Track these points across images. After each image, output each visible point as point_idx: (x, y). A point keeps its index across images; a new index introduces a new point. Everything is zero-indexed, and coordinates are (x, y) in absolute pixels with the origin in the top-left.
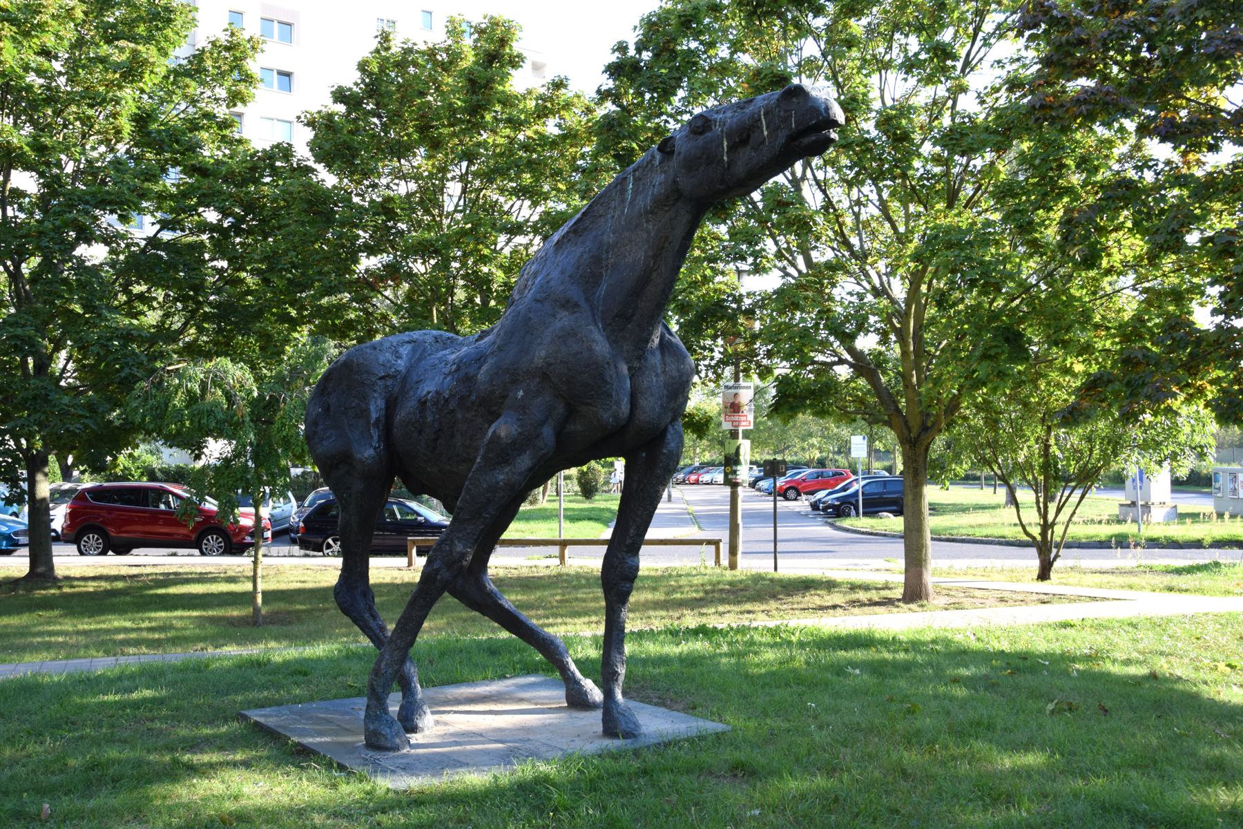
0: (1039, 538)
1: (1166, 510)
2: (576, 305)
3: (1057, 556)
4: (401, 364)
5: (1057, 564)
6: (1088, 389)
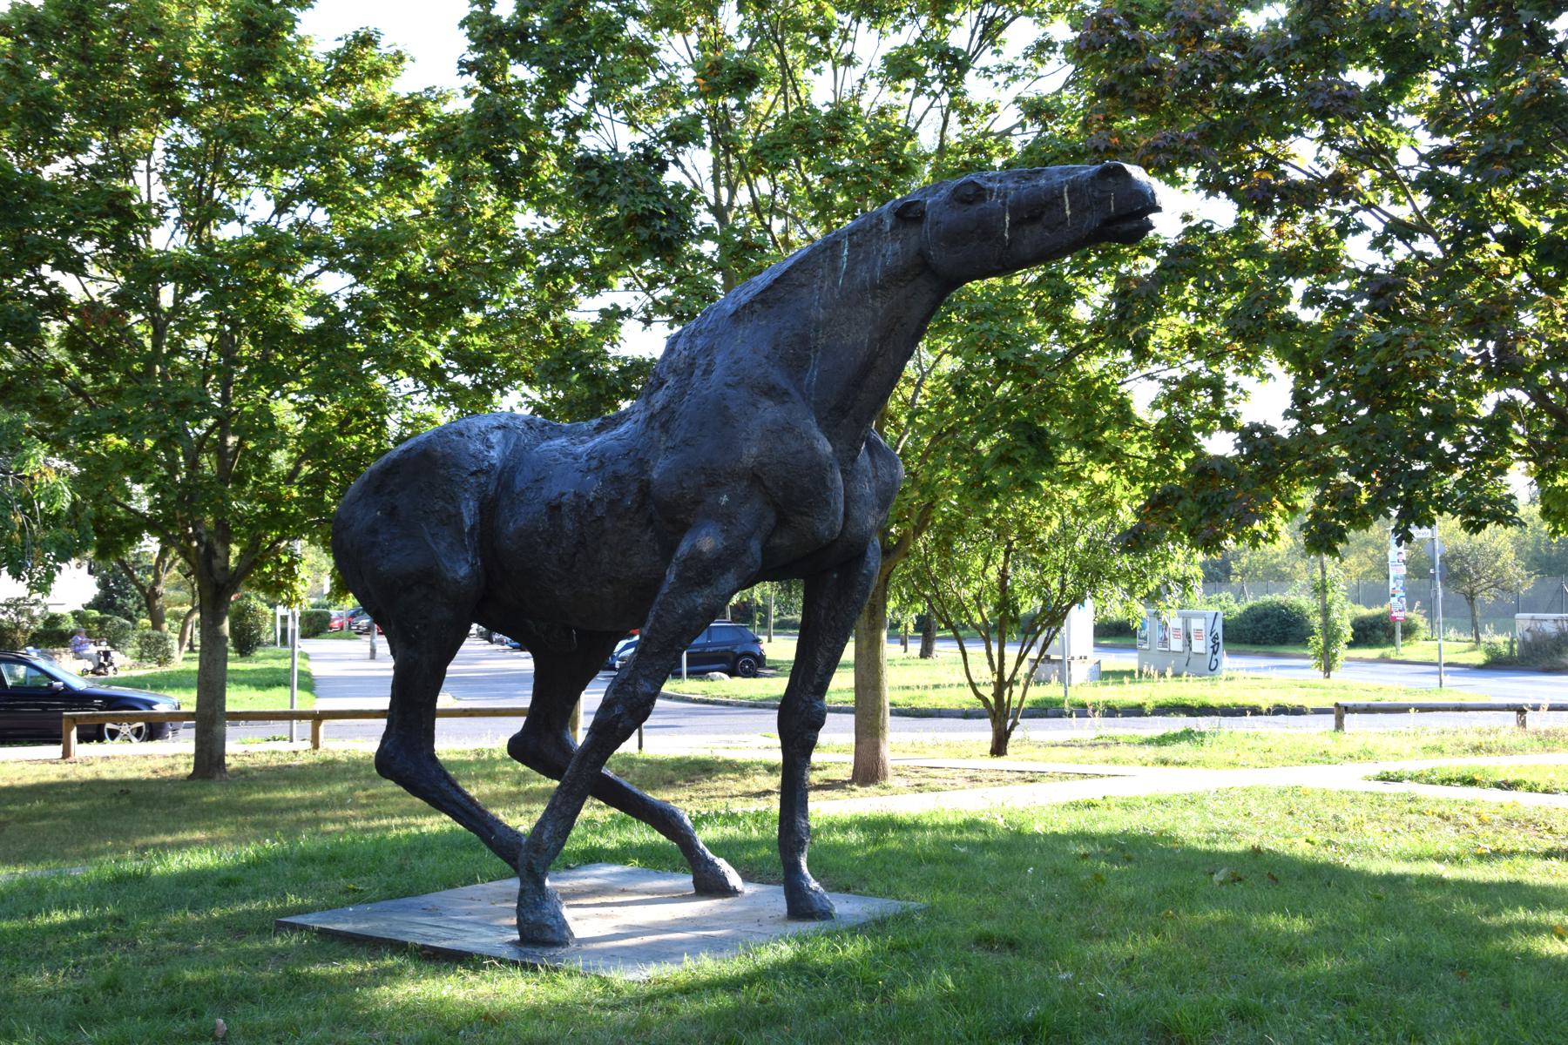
0: (992, 700)
1: (1089, 665)
2: (786, 393)
3: (1014, 724)
4: (495, 455)
5: (1015, 735)
6: (1153, 507)
